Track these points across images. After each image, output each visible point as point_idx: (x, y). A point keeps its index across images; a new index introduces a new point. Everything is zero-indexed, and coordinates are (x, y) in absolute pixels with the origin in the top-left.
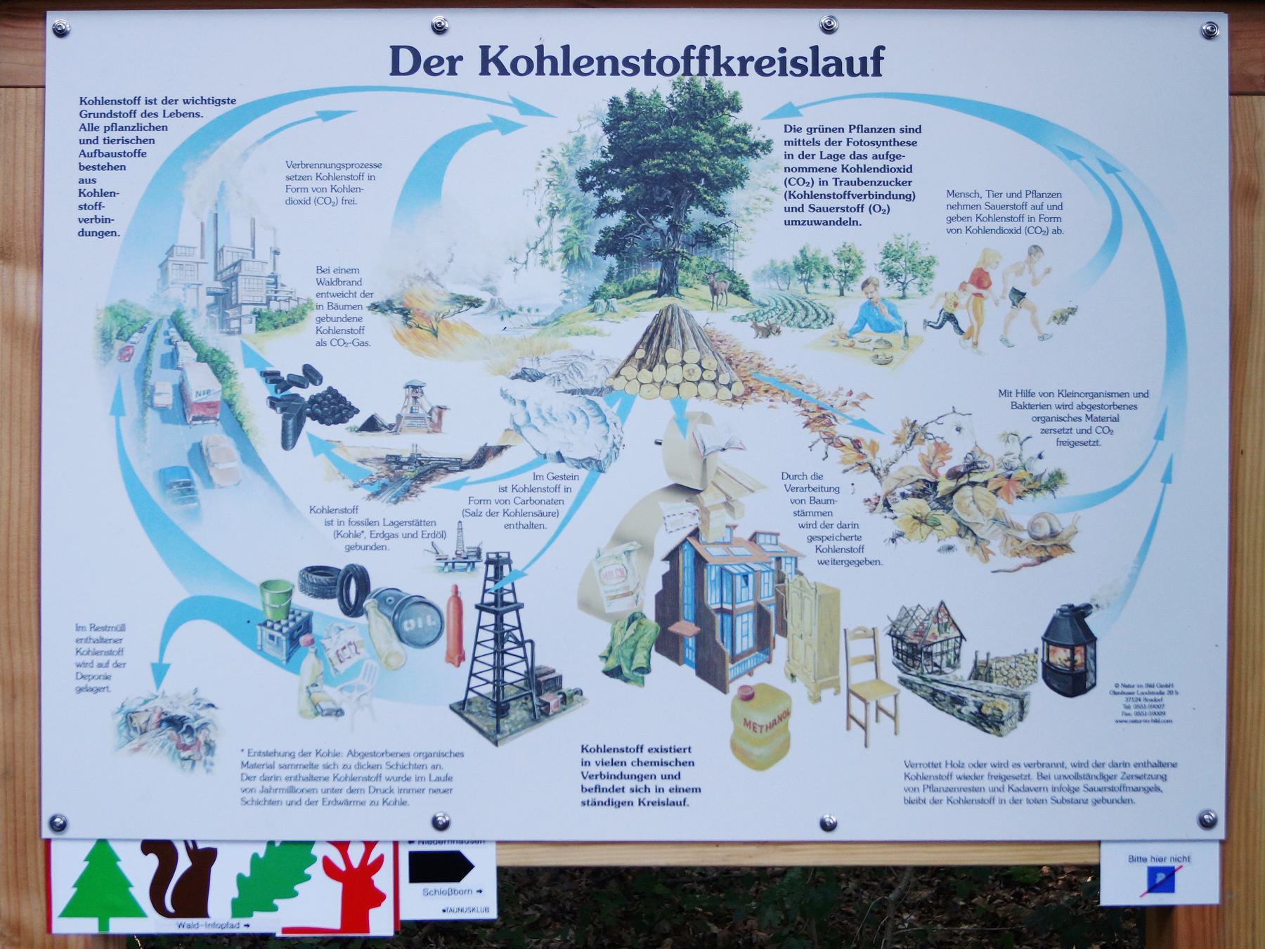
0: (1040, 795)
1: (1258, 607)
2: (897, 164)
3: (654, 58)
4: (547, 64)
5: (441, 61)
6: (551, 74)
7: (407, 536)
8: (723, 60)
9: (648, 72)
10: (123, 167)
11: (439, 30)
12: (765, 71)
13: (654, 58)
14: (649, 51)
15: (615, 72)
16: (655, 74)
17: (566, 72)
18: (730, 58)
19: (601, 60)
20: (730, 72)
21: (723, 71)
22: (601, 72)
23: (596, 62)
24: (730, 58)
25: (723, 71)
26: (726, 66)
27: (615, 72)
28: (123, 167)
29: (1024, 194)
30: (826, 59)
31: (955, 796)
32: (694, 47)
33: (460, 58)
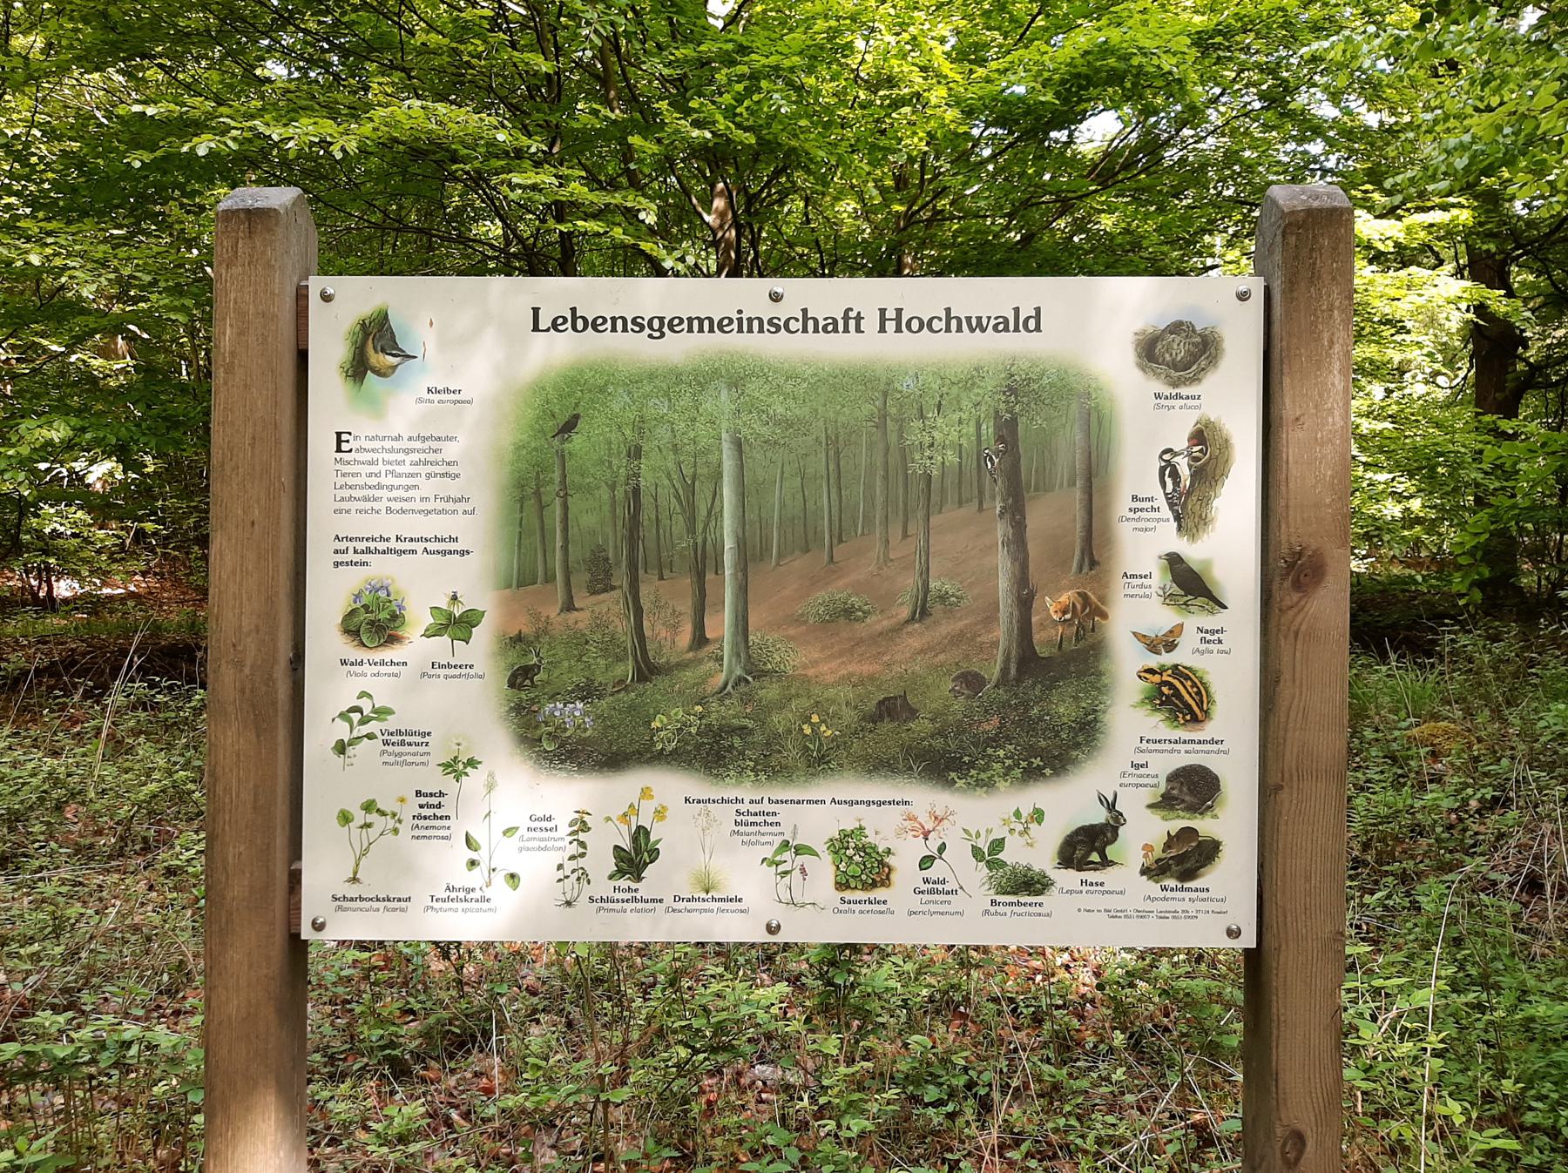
2: (439, 457)
4: (811, 324)
5: (681, 321)
10: (365, 564)
11: (776, 298)
12: (676, 328)
15: (761, 330)
17: (1017, 329)
19: (614, 319)
22: (614, 329)
23: (609, 321)
28: (365, 564)
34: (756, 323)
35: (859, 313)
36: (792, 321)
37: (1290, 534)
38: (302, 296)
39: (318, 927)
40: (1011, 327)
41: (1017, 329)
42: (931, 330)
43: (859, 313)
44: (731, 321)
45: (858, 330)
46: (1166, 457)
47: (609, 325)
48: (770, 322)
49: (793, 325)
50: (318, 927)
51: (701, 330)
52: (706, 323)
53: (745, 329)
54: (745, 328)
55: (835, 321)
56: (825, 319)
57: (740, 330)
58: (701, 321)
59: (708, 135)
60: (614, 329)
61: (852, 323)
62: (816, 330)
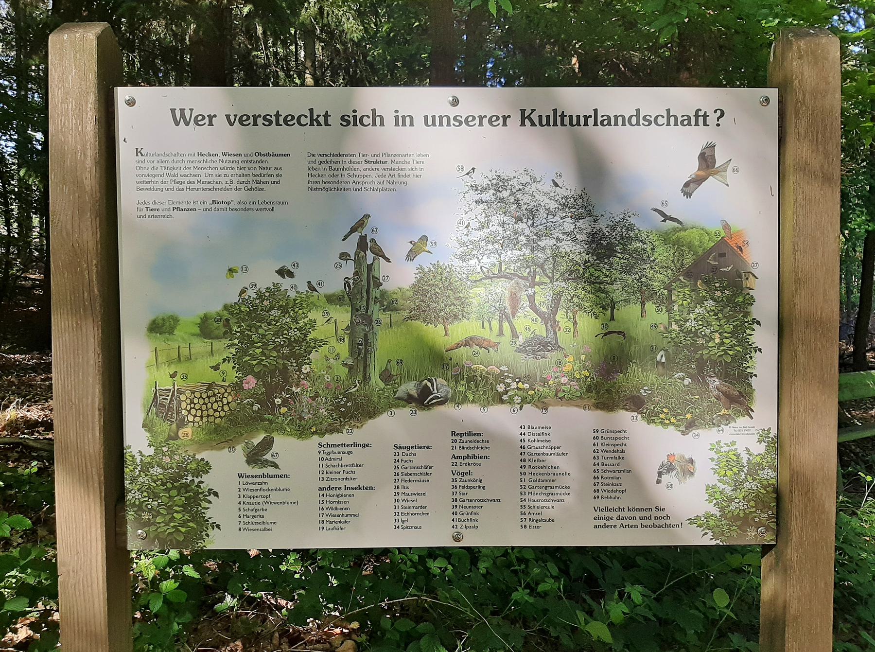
0: (632, 522)
3: (281, 115)
4: (672, 119)
5: (474, 118)
6: (622, 125)
8: (315, 117)
9: (278, 124)
13: (281, 115)
14: (278, 112)
16: (281, 125)
17: (555, 124)
18: (318, 116)
20: (319, 124)
24: (318, 116)
26: (529, 117)
27: (449, 124)
30: (602, 116)
31: (625, 522)
32: (700, 110)
33: (215, 116)
34: (620, 119)
35: (705, 112)
36: (365, 118)
37: (841, 382)
42: (656, 124)
43: (705, 112)
46: (346, 280)
48: (455, 119)
53: (400, 123)
55: (689, 118)
56: (682, 116)
61: (701, 119)
62: (676, 124)
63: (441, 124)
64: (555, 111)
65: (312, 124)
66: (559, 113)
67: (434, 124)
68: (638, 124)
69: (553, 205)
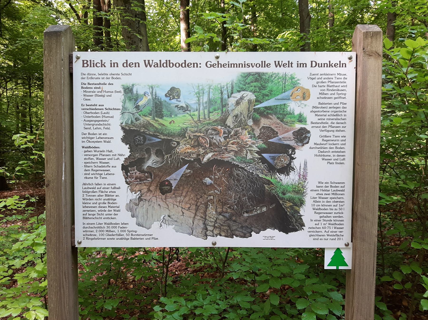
1: (65, 300)
4: (220, 65)
5: (191, 64)
7: (147, 239)
8: (103, 63)
17: (160, 67)
19: (135, 63)
21: (103, 66)
22: (194, 67)
25: (103, 66)
26: (104, 65)
29: (339, 103)
38: (71, 57)
39: (80, 243)
40: (159, 66)
41: (160, 67)
44: (226, 65)
45: (292, 67)
47: (192, 65)
49: (98, 65)
50: (80, 243)
51: (234, 67)
52: (235, 65)
54: (299, 66)
57: (229, 67)
58: (234, 65)
59: (328, 23)
60: (194, 67)
63: (231, 67)
64: (289, 62)
65: (102, 67)
66: (290, 62)
67: (321, 66)
68: (185, 67)
69: (343, 317)
